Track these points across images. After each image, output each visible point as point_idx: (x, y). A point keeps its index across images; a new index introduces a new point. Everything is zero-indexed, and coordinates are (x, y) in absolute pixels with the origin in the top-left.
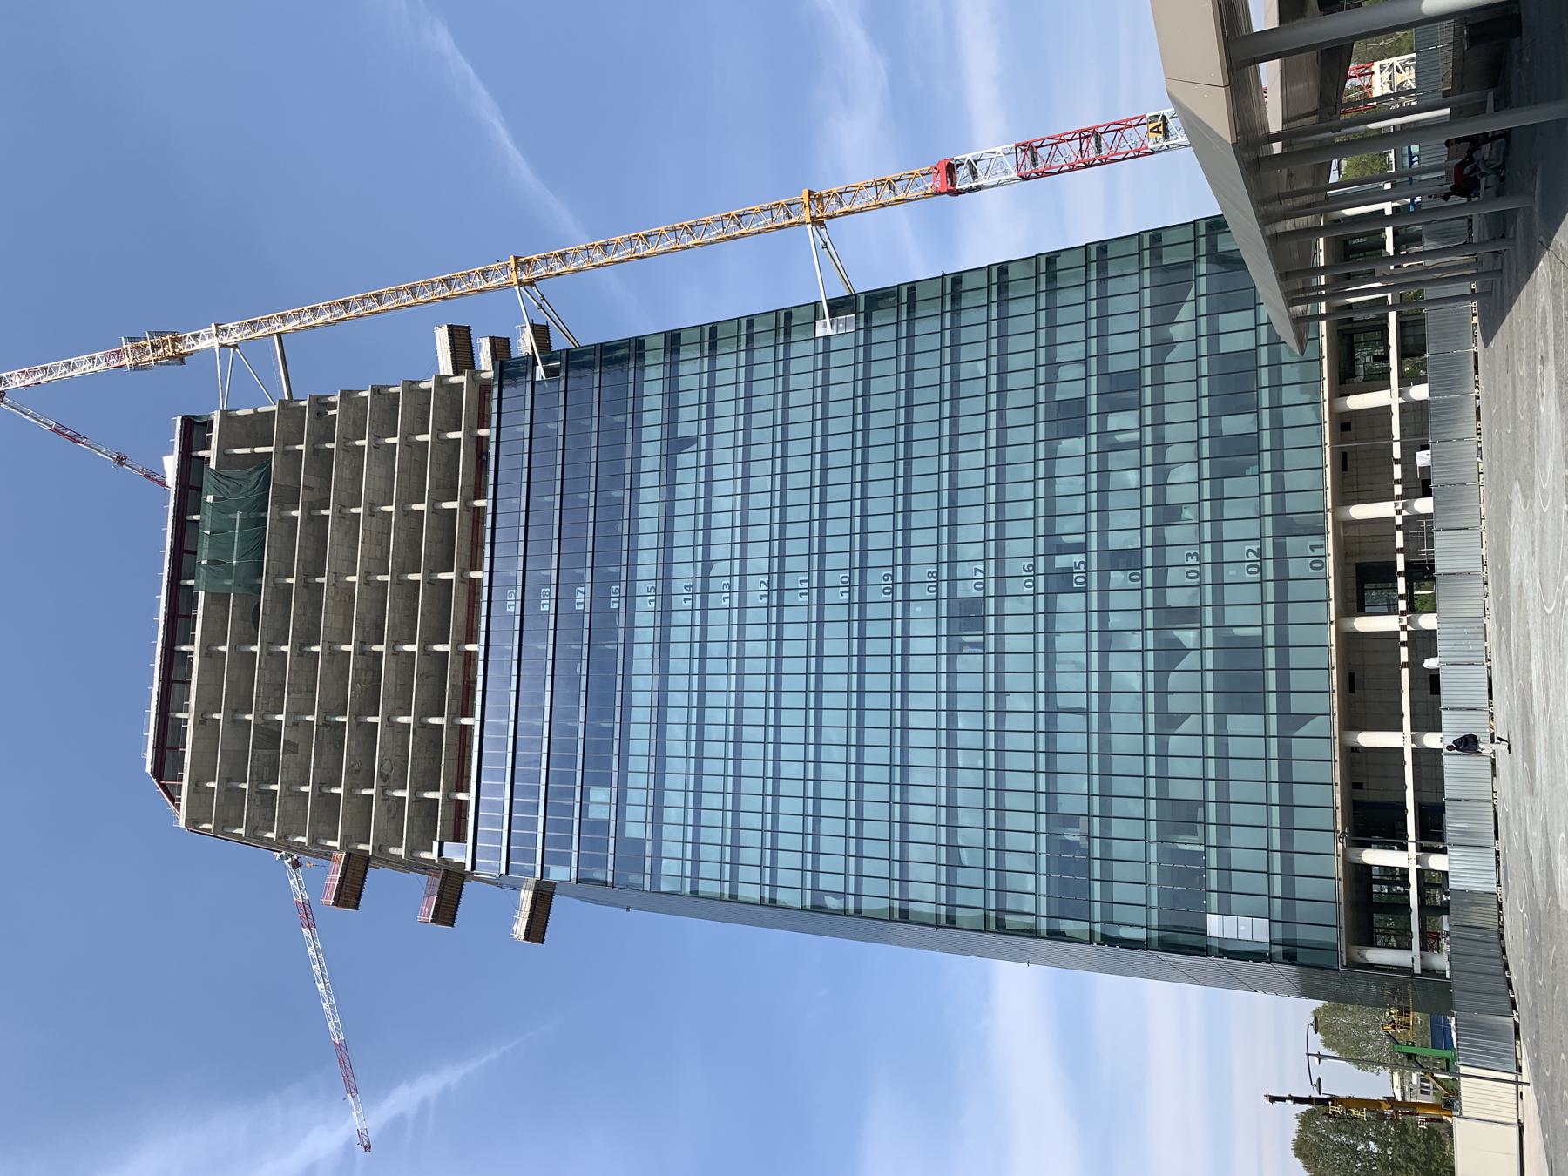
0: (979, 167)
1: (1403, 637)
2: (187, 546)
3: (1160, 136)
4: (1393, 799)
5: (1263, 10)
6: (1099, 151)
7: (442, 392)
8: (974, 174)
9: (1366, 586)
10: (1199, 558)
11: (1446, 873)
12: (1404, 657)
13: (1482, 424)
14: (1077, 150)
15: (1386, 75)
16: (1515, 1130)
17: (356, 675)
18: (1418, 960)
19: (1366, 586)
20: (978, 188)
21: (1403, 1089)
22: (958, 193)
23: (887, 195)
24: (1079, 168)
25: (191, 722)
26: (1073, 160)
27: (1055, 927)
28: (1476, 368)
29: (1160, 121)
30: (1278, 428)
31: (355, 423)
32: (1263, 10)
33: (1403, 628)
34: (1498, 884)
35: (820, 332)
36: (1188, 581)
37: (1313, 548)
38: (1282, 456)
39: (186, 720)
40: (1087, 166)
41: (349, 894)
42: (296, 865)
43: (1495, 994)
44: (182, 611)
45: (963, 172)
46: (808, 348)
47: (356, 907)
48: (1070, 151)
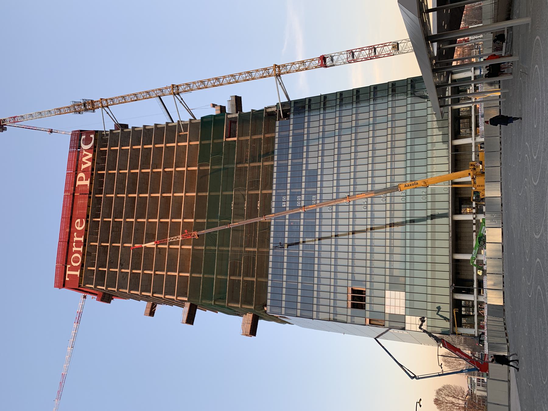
0: (334, 58)
1: (474, 221)
4: (470, 278)
5: (431, 1)
7: (145, 131)
8: (332, 60)
9: (462, 206)
12: (474, 229)
13: (502, 151)
14: (368, 53)
17: (112, 229)
18: (476, 332)
19: (462, 206)
20: (334, 65)
22: (326, 67)
26: (366, 56)
27: (336, 318)
31: (115, 141)
32: (431, 1)
33: (474, 219)
36: (401, 202)
40: (371, 59)
41: (190, 320)
42: (85, 297)
45: (328, 60)
47: (192, 324)
48: (365, 53)
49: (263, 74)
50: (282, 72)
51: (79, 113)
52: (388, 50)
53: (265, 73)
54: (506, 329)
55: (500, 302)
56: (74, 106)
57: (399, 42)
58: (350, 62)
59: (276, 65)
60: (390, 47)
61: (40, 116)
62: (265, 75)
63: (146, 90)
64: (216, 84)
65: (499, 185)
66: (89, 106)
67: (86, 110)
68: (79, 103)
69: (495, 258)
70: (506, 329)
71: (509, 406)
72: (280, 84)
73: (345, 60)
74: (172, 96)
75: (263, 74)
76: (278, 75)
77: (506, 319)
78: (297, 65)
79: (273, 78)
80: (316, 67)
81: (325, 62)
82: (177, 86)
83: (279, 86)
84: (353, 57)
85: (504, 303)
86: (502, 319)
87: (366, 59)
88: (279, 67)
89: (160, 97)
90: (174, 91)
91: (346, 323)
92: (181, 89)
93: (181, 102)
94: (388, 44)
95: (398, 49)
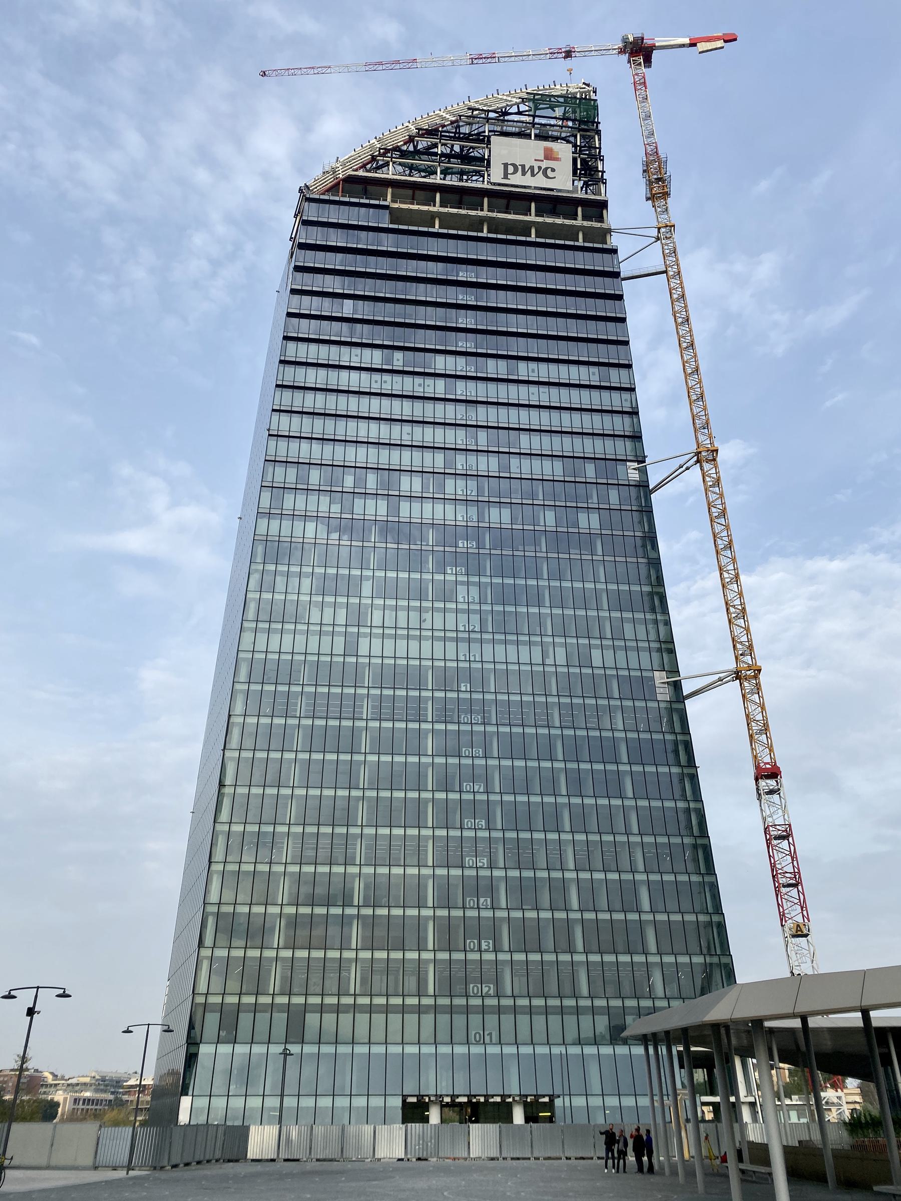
0: (776, 797)
2: (513, 203)
3: (794, 931)
6: (784, 886)
8: (771, 792)
10: (486, 951)
11: (428, 1122)
13: (510, 1161)
15: (836, 1100)
16: (43, 1162)
21: (77, 1084)
22: (757, 779)
23: (755, 727)
24: (773, 871)
25: (480, 213)
26: (778, 866)
28: (549, 1158)
29: (805, 932)
30: (578, 1011)
34: (318, 1160)
35: (657, 674)
37: (490, 1034)
38: (540, 1014)
39: (482, 210)
40: (773, 877)
43: (182, 1156)
44: (466, 198)
45: (772, 783)
46: (645, 664)
48: (785, 864)
49: (734, 606)
50: (746, 684)
51: (644, 171)
52: (784, 864)
53: (743, 648)
54: (199, 1163)
55: (253, 1151)
56: (659, 160)
57: (809, 937)
58: (766, 830)
59: (759, 671)
60: (799, 919)
61: (643, 115)
62: (739, 646)
63: (701, 367)
64: (713, 510)
65: (494, 1153)
66: (658, 188)
67: (650, 183)
68: (663, 171)
69: (311, 1140)
70: (199, 1163)
71: (48, 1168)
72: (720, 680)
73: (770, 819)
74: (694, 448)
75: (734, 606)
76: (738, 675)
77: (218, 1165)
78: (759, 717)
79: (732, 665)
80: (756, 757)
81: (768, 777)
82: (714, 460)
83: (716, 677)
84: (776, 838)
85: (253, 1160)
86: (218, 1155)
87: (773, 867)
88: (756, 677)
89: (665, 272)
90: (704, 454)
91: (214, 822)
92: (707, 466)
93: (681, 467)
94: (795, 863)
95: (794, 936)
